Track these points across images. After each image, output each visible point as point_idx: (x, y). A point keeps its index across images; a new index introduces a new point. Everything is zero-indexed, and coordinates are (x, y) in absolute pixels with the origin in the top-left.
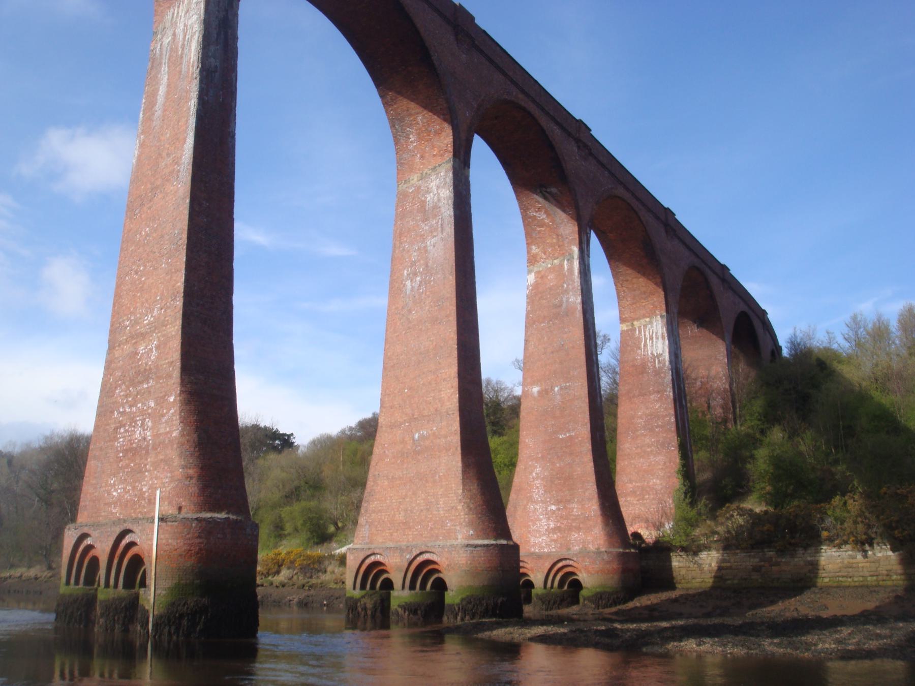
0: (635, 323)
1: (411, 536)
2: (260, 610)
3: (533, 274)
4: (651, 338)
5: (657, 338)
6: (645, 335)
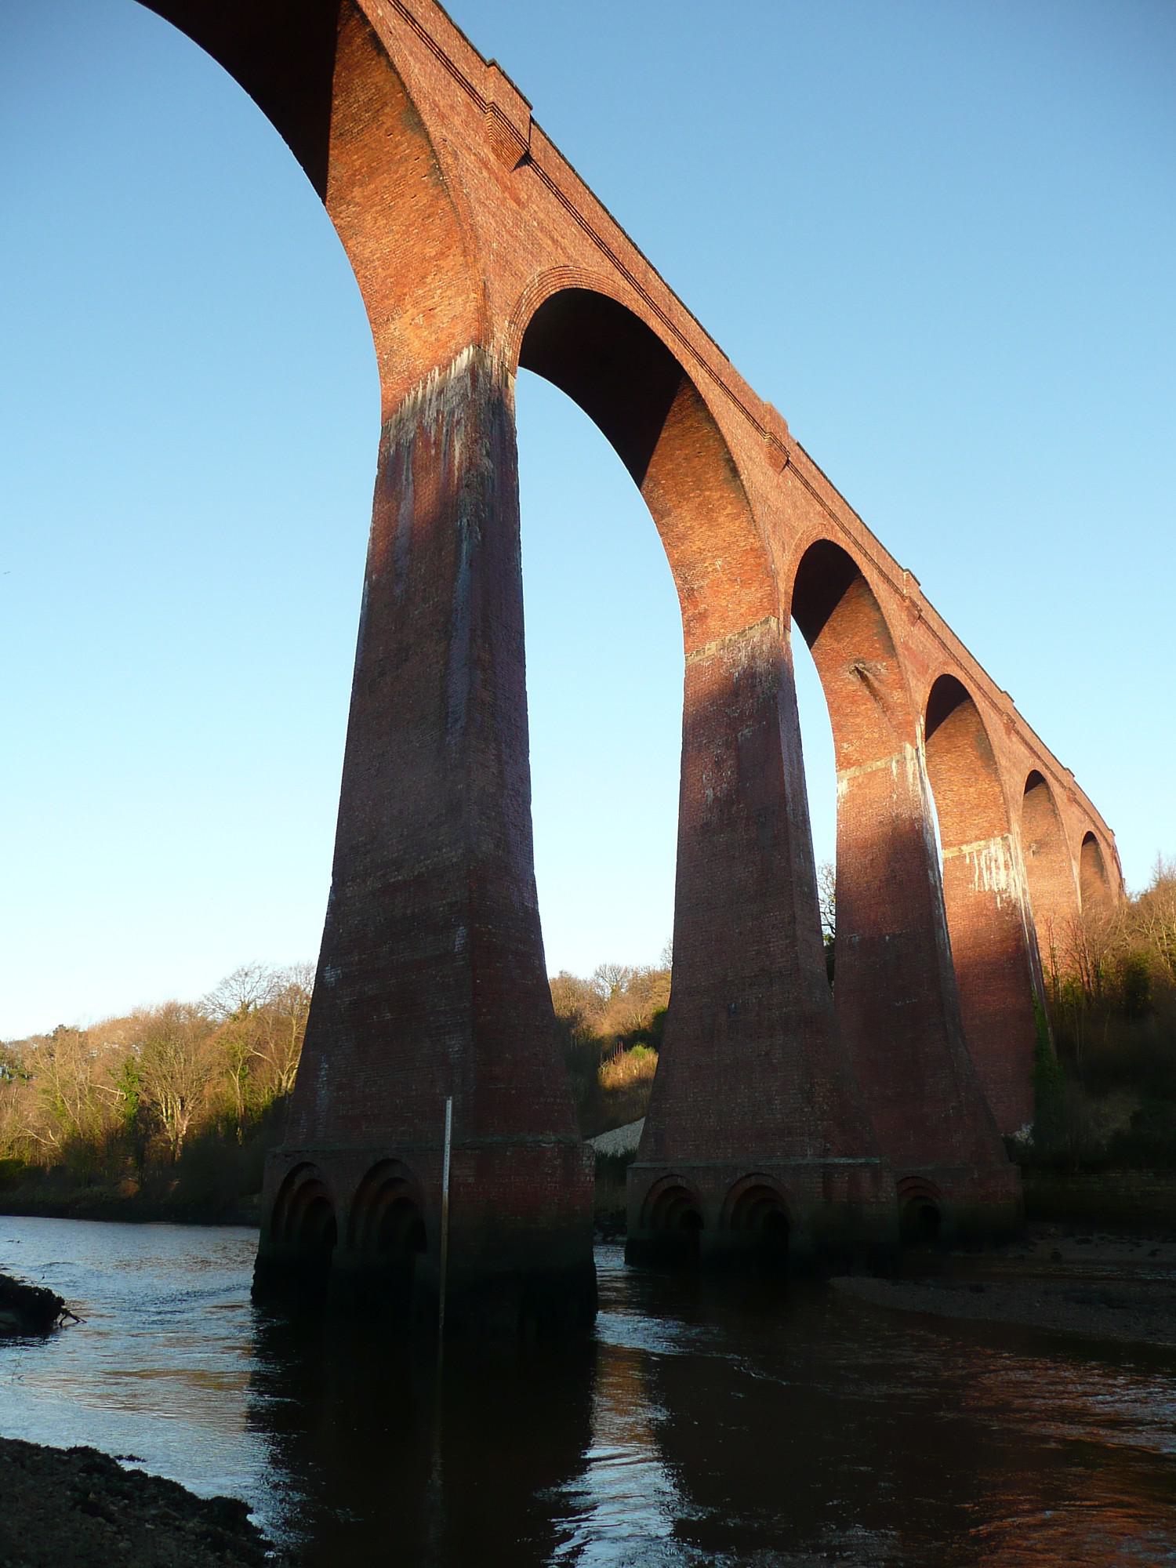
0: (964, 847)
1: (730, 1151)
2: (309, 990)
3: (845, 782)
4: (989, 868)
5: (998, 868)
6: (979, 864)
